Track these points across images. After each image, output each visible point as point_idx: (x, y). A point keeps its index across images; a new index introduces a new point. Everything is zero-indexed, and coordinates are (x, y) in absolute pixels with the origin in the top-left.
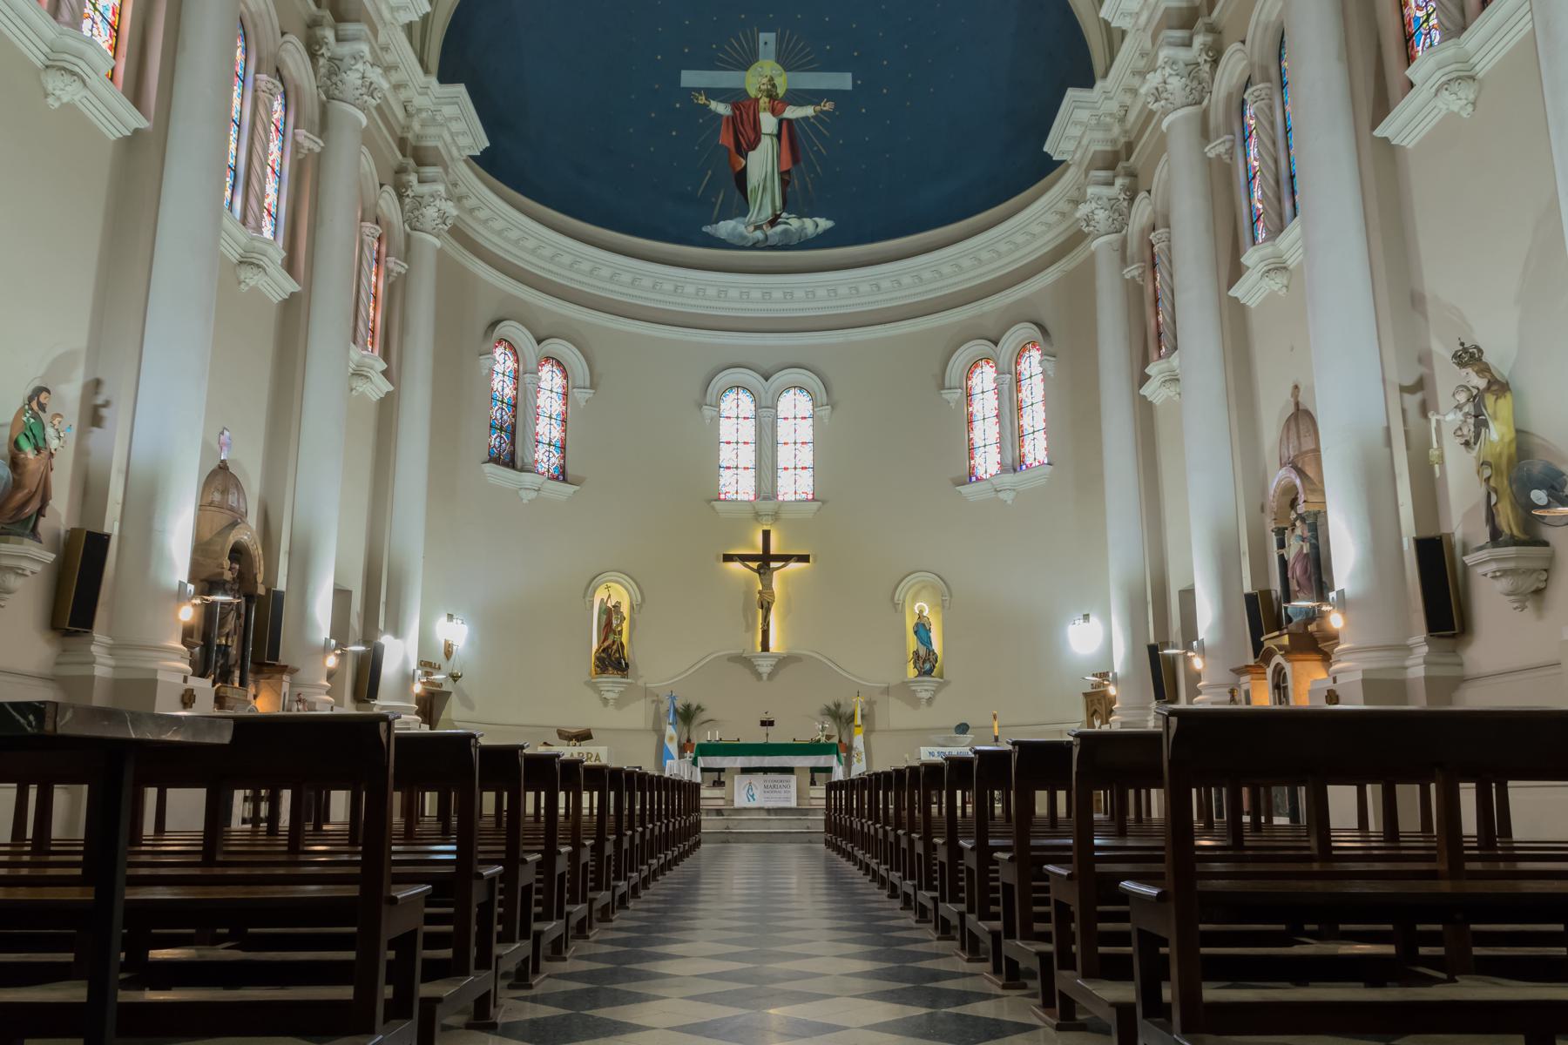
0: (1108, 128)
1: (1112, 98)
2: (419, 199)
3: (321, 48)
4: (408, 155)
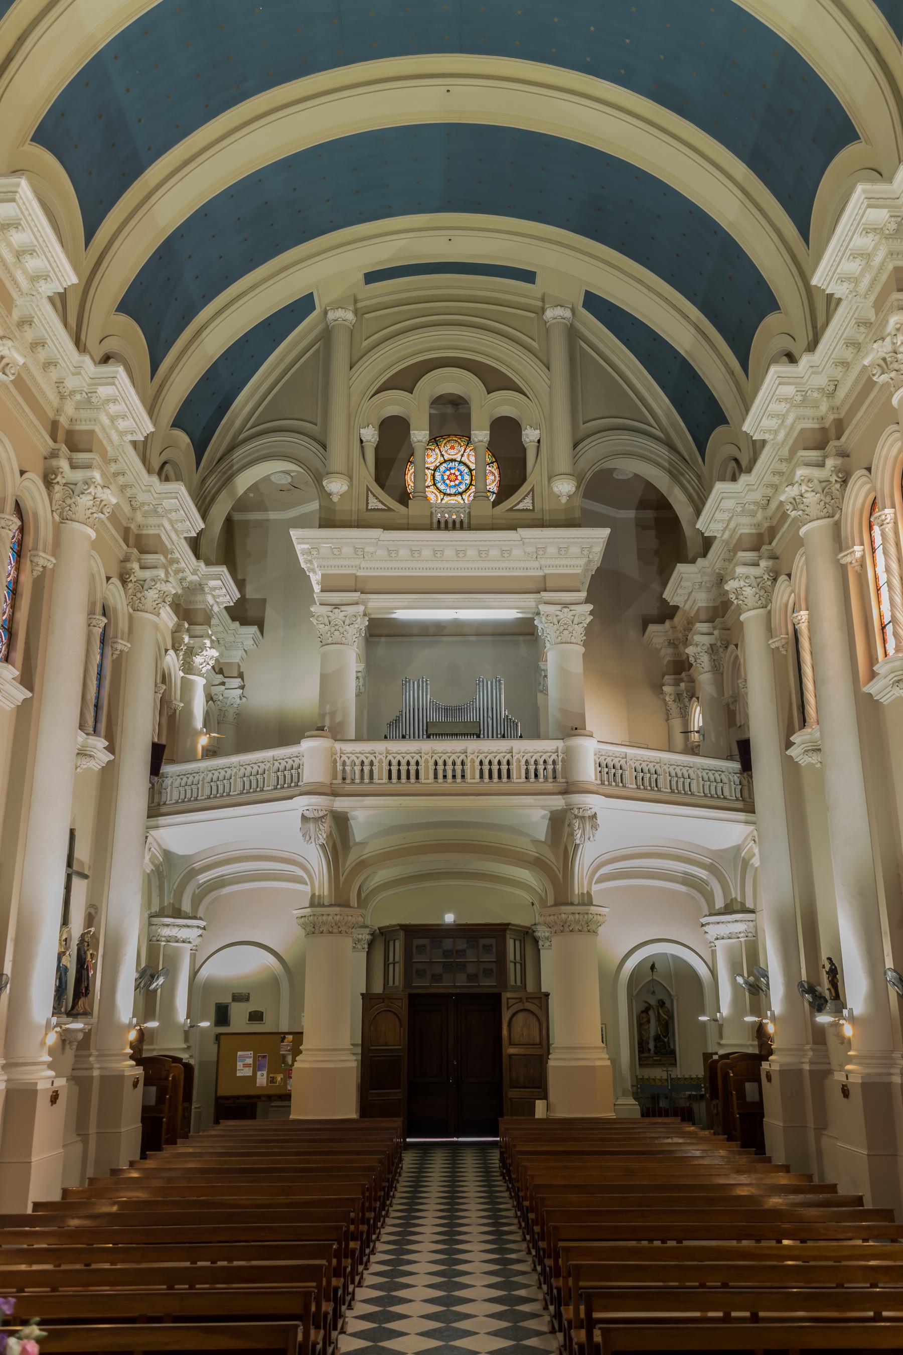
0: (753, 514)
1: (820, 373)
2: (142, 582)
3: (56, 476)
4: (58, 440)
